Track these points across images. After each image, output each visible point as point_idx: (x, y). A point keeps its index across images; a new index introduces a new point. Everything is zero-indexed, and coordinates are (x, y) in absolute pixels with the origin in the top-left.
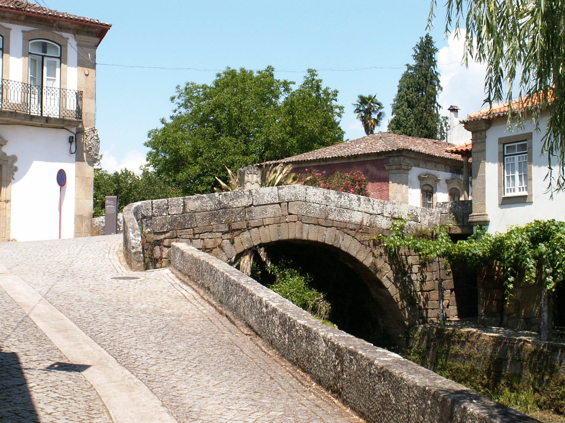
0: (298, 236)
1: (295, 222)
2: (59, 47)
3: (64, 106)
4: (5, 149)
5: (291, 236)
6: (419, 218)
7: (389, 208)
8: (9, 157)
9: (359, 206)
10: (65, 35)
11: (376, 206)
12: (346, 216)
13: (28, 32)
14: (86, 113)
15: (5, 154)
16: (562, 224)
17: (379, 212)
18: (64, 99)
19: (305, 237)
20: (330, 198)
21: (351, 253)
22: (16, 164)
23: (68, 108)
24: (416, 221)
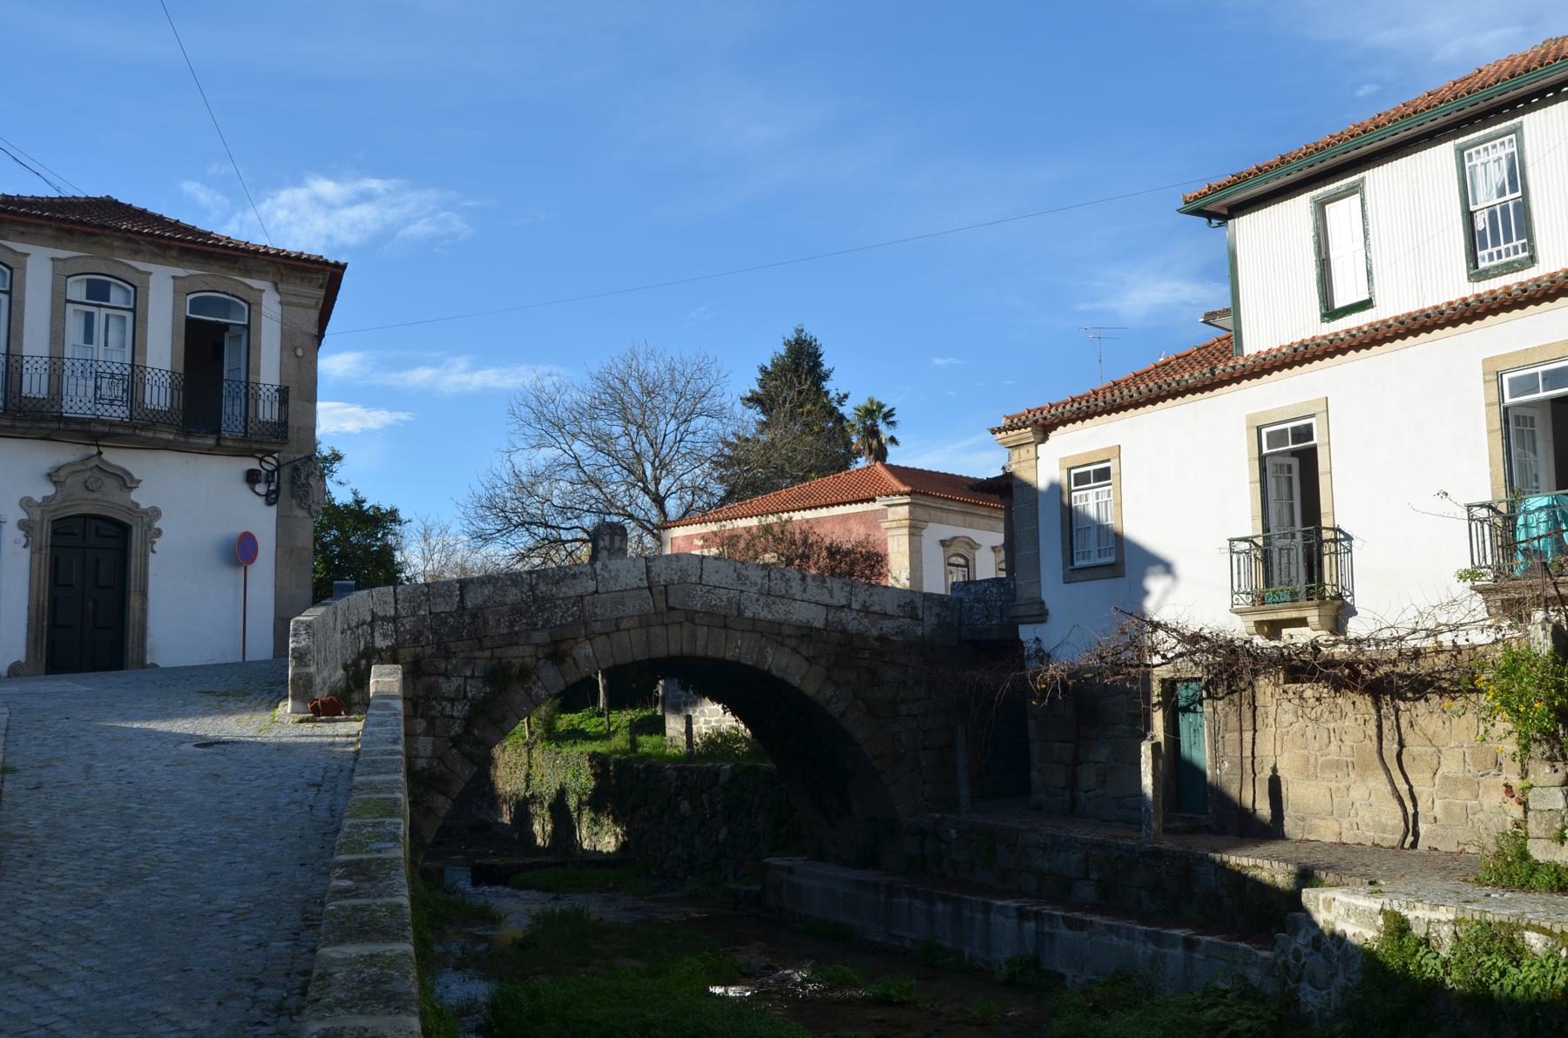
0: (686, 650)
1: (607, 634)
2: (245, 306)
3: (140, 399)
4: (135, 496)
5: (674, 650)
6: (920, 612)
7: (861, 596)
8: (145, 512)
9: (804, 591)
10: (255, 283)
11: (837, 591)
12: (778, 612)
13: (184, 278)
14: (299, 429)
15: (137, 505)
16: (1564, 38)
17: (843, 602)
18: (252, 402)
19: (700, 652)
20: (747, 578)
21: (790, 680)
22: (157, 525)
23: (25, 391)
24: (914, 617)
